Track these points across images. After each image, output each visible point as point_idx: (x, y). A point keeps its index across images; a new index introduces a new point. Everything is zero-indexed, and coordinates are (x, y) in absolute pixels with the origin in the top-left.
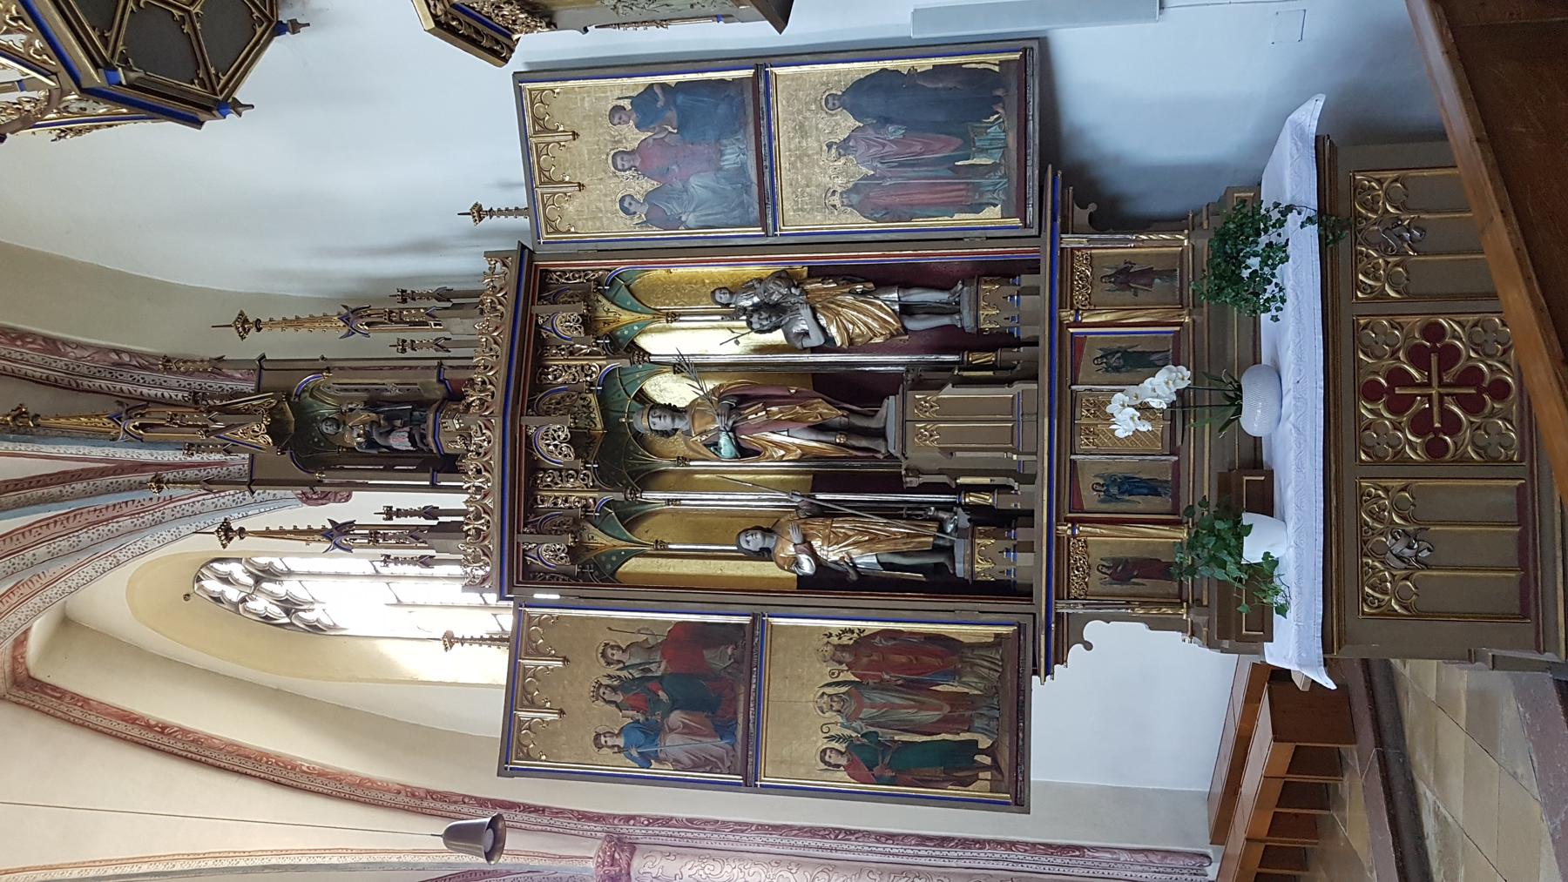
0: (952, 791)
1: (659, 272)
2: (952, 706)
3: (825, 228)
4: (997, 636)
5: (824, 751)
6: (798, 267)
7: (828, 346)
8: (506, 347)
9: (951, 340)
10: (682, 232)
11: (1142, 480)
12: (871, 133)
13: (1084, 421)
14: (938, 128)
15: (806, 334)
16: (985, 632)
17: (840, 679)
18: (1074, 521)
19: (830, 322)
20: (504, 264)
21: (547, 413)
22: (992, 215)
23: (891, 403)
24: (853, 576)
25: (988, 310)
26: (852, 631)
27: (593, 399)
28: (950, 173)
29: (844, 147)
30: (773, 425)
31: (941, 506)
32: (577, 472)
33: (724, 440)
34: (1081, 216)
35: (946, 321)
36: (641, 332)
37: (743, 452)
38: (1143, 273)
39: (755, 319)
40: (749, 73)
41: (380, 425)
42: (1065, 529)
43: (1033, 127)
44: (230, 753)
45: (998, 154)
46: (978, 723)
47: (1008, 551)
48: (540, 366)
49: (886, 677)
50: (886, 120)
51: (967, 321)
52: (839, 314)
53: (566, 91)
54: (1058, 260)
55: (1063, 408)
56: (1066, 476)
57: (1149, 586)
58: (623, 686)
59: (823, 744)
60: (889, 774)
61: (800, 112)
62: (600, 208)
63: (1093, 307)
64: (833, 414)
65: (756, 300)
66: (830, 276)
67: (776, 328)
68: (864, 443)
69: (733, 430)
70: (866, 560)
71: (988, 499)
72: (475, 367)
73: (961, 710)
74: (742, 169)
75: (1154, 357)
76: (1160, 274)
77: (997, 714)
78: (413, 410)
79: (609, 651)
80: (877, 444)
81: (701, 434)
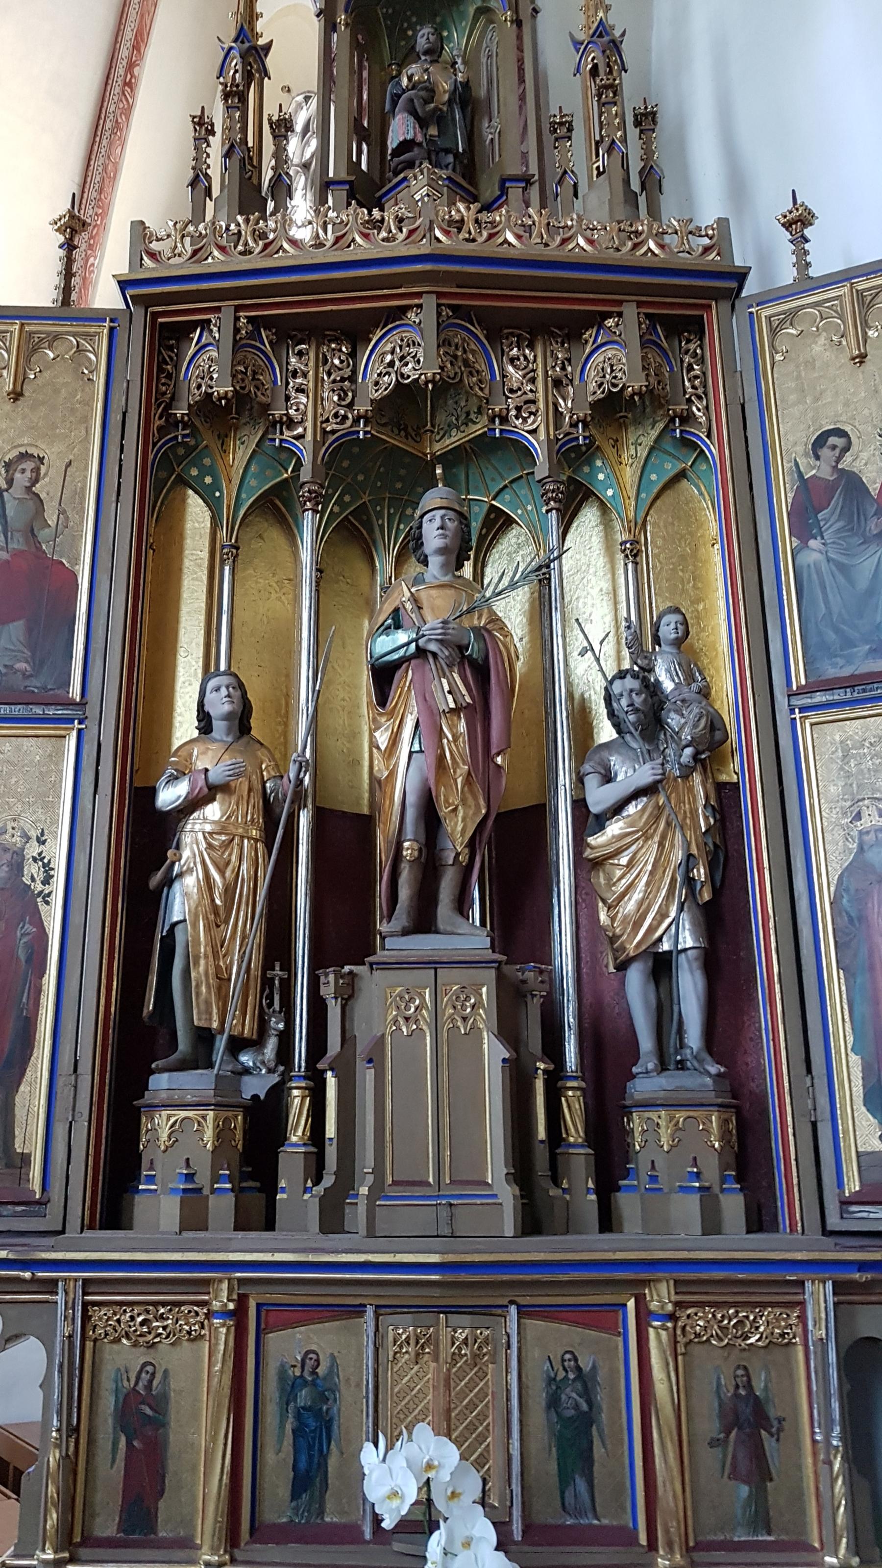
1: (712, 526)
3: (813, 800)
4: (26, 1159)
6: (735, 764)
7: (586, 821)
9: (609, 1056)
10: (788, 542)
11: (324, 1457)
13: (445, 1334)
15: (608, 778)
16: (29, 1134)
20: (707, 250)
21: (443, 343)
24: (155, 879)
25: (672, 1129)
26: (46, 881)
27: (478, 428)
30: (430, 728)
31: (286, 1039)
32: (350, 406)
33: (402, 637)
35: (646, 1043)
36: (604, 508)
37: (384, 675)
38: (759, 1456)
39: (630, 683)
41: (426, 102)
42: (222, 1298)
44: (105, 170)
47: (189, 1177)
48: (538, 328)
51: (645, 1085)
52: (647, 837)
55: (468, 1291)
56: (334, 1302)
57: (110, 1472)
63: (680, 1349)
64: (458, 828)
65: (668, 686)
68: (404, 893)
69: (421, 653)
70: (182, 902)
75: (581, 1484)
76: (759, 1496)
78: (456, 155)
79: (29, 465)
81: (415, 599)
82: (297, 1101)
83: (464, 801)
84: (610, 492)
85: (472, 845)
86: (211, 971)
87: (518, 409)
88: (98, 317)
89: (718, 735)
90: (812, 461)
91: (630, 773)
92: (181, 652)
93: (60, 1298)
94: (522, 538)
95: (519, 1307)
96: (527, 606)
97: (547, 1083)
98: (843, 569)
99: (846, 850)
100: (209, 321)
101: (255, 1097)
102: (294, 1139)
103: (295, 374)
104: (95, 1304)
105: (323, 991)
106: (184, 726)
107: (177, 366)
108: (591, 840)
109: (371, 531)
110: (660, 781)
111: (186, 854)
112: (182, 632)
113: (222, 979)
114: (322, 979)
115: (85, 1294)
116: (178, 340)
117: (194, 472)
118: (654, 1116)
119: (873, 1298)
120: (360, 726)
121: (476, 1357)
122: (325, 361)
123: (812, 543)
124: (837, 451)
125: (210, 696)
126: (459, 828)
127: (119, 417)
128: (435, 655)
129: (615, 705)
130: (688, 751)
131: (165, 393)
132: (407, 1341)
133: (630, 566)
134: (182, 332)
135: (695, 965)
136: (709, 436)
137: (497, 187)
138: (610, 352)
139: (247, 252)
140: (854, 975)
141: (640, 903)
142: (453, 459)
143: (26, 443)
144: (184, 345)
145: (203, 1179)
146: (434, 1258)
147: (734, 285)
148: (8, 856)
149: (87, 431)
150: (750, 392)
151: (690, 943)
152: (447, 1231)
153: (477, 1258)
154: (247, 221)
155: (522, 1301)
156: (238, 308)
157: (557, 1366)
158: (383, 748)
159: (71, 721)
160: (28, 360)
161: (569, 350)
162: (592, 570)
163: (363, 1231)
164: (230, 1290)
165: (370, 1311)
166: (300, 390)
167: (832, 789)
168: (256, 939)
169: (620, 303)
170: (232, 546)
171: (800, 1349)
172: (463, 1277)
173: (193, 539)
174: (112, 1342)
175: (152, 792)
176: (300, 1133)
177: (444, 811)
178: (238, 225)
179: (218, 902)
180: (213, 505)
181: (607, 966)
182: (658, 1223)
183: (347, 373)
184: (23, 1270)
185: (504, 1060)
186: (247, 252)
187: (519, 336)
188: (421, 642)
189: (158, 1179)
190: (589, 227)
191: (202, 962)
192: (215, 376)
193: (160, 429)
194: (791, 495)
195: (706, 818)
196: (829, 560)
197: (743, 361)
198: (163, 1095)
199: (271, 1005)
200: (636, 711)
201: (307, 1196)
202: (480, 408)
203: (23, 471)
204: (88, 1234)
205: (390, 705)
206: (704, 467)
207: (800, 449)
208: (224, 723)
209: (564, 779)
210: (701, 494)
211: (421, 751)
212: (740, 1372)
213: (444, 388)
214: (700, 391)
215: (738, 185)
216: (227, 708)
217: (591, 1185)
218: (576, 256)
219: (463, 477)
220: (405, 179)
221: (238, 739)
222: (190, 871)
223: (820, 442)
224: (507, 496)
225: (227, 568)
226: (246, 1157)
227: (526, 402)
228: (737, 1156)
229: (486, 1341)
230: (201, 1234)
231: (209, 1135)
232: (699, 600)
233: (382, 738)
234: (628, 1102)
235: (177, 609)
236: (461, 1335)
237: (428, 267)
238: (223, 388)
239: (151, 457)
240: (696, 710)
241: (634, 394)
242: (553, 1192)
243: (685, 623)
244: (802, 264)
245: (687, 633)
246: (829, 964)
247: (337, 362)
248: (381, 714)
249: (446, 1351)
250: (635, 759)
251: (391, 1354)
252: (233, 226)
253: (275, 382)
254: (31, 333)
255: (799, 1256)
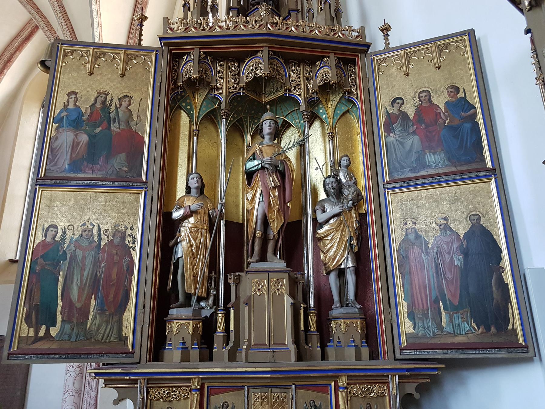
0: (22, 310)
1: (357, 128)
2: (80, 309)
4: (126, 338)
5: (56, 227)
6: (365, 207)
8: (310, 36)
9: (324, 303)
12: (456, 245)
13: (271, 395)
14: (464, 287)
15: (324, 211)
16: (128, 330)
17: (103, 236)
18: (201, 390)
19: (332, 225)
20: (357, 37)
21: (270, 64)
22: (407, 326)
23: (282, 264)
24: (172, 243)
25: (344, 326)
26: (134, 242)
27: (280, 93)
28: (433, 298)
29: (445, 228)
30: (266, 193)
31: (216, 297)
32: (238, 84)
33: (256, 162)
34: (411, 388)
35: (336, 298)
36: (322, 122)
37: (250, 175)
40: (489, 165)
42: (195, 384)
43: (471, 355)
44: (143, 3)
45: (449, 329)
46: (68, 327)
47: (184, 344)
49: (102, 265)
50: (466, 254)
51: (337, 311)
52: (337, 230)
53: (465, 60)
54: (380, 373)
58: (105, 108)
59: (61, 226)
60: (38, 268)
61: (466, 198)
62: (394, 87)
64: (275, 226)
65: (344, 181)
66: (360, 226)
67: (328, 195)
68: (256, 248)
69: (263, 168)
70: (181, 251)
71: (220, 329)
72: (298, 21)
73: (77, 315)
74: (425, 166)
77: (73, 338)
79: (127, 99)
80: (256, 256)
81: (260, 150)
82: (220, 318)
83: (277, 218)
84: (324, 116)
85: (279, 233)
86: (192, 274)
87: (295, 87)
88: (149, 49)
89: (360, 197)
90: (391, 108)
91: (331, 210)
92: (179, 166)
93: (139, 385)
94: (294, 131)
95: (296, 385)
96: (295, 154)
97: (304, 311)
98: (402, 143)
99: (402, 234)
100: (190, 53)
101: (206, 317)
102: (219, 331)
103: (219, 72)
104: (151, 387)
105: (229, 281)
106: (181, 191)
107: (178, 68)
108: (319, 232)
109: (243, 127)
110: (341, 212)
111: (183, 234)
112: (179, 159)
113: (195, 277)
114: (229, 277)
115: (147, 384)
116: (179, 59)
117: (184, 104)
118: (339, 321)
119: (411, 381)
120: (239, 193)
121: (282, 402)
122: (230, 68)
123: (391, 134)
124: (399, 105)
125: (190, 181)
126: (276, 226)
127: (159, 84)
128: (267, 169)
129: (327, 187)
130: (351, 202)
131: (174, 77)
132: (258, 397)
133: (331, 141)
134: (180, 56)
135: (353, 272)
136: (357, 99)
137: (287, 12)
138: (325, 69)
139: (204, 30)
140: (404, 276)
141: (335, 252)
142: (273, 103)
143: (126, 92)
144: (181, 60)
145: (188, 344)
146: (269, 369)
147: (366, 49)
148: (120, 234)
149: (148, 88)
150: (371, 84)
151: (351, 265)
152: (272, 360)
153: (283, 369)
154: (204, 19)
155: (297, 383)
156: (200, 49)
157: (308, 405)
158: (249, 200)
159: (143, 188)
160: (127, 63)
161: (311, 68)
162: (318, 142)
163: (244, 361)
164: (198, 382)
165: (246, 388)
166: (221, 78)
167: (397, 215)
168: (206, 264)
169: (329, 53)
170: (197, 130)
171: (387, 397)
172: (278, 375)
173: (183, 127)
174: (157, 400)
175: (171, 214)
176: (221, 328)
177: (270, 221)
178: (201, 20)
179: (194, 251)
180: (190, 116)
181: (322, 273)
182: (340, 357)
183: (237, 72)
184: (126, 376)
185: (291, 303)
186: (204, 30)
187: (295, 63)
188: (263, 164)
189: (173, 345)
190: (317, 26)
191: (189, 271)
192: (192, 71)
193: (172, 89)
194: (384, 119)
195: (356, 224)
196: (397, 140)
197: (369, 74)
198: (175, 316)
199: (211, 286)
200: (334, 189)
201: (224, 350)
202: (281, 86)
203: (125, 101)
204: (148, 363)
205: (252, 185)
206: (355, 109)
207: (387, 103)
208: (195, 190)
209: (310, 211)
210: (354, 118)
211: (263, 201)
212: (368, 406)
213: (270, 79)
214: (354, 83)
215: (364, 16)
216: (196, 185)
217: (318, 345)
218: (315, 37)
219: (275, 110)
220: (257, 8)
221: (200, 196)
222: (184, 240)
223: (394, 101)
224: (289, 117)
225: (195, 138)
226: (203, 337)
227: (297, 85)
228: (366, 335)
229: (285, 397)
230: (188, 363)
231: (190, 329)
232: (353, 153)
233: (250, 197)
234: (331, 318)
235: (178, 152)
236: (276, 395)
237: (266, 37)
238: (195, 75)
239: (170, 98)
240: (353, 189)
241: (333, 83)
242: (306, 347)
243: (349, 160)
244: (387, 43)
245: (350, 163)
246: (396, 272)
247: (233, 68)
248: (249, 188)
249: (271, 401)
250: (334, 205)
251: (253, 402)
252: (199, 21)
253: (212, 74)
254: (128, 54)
255: (388, 367)
